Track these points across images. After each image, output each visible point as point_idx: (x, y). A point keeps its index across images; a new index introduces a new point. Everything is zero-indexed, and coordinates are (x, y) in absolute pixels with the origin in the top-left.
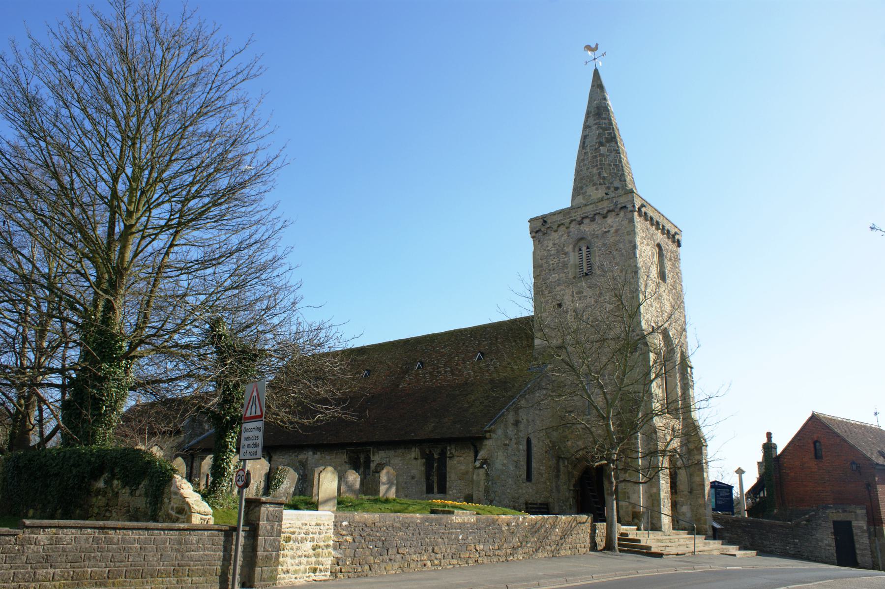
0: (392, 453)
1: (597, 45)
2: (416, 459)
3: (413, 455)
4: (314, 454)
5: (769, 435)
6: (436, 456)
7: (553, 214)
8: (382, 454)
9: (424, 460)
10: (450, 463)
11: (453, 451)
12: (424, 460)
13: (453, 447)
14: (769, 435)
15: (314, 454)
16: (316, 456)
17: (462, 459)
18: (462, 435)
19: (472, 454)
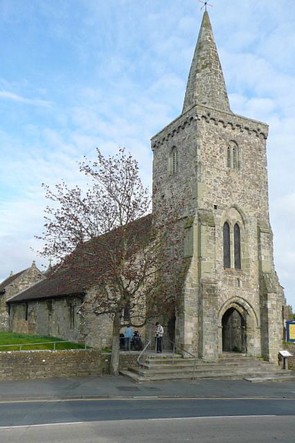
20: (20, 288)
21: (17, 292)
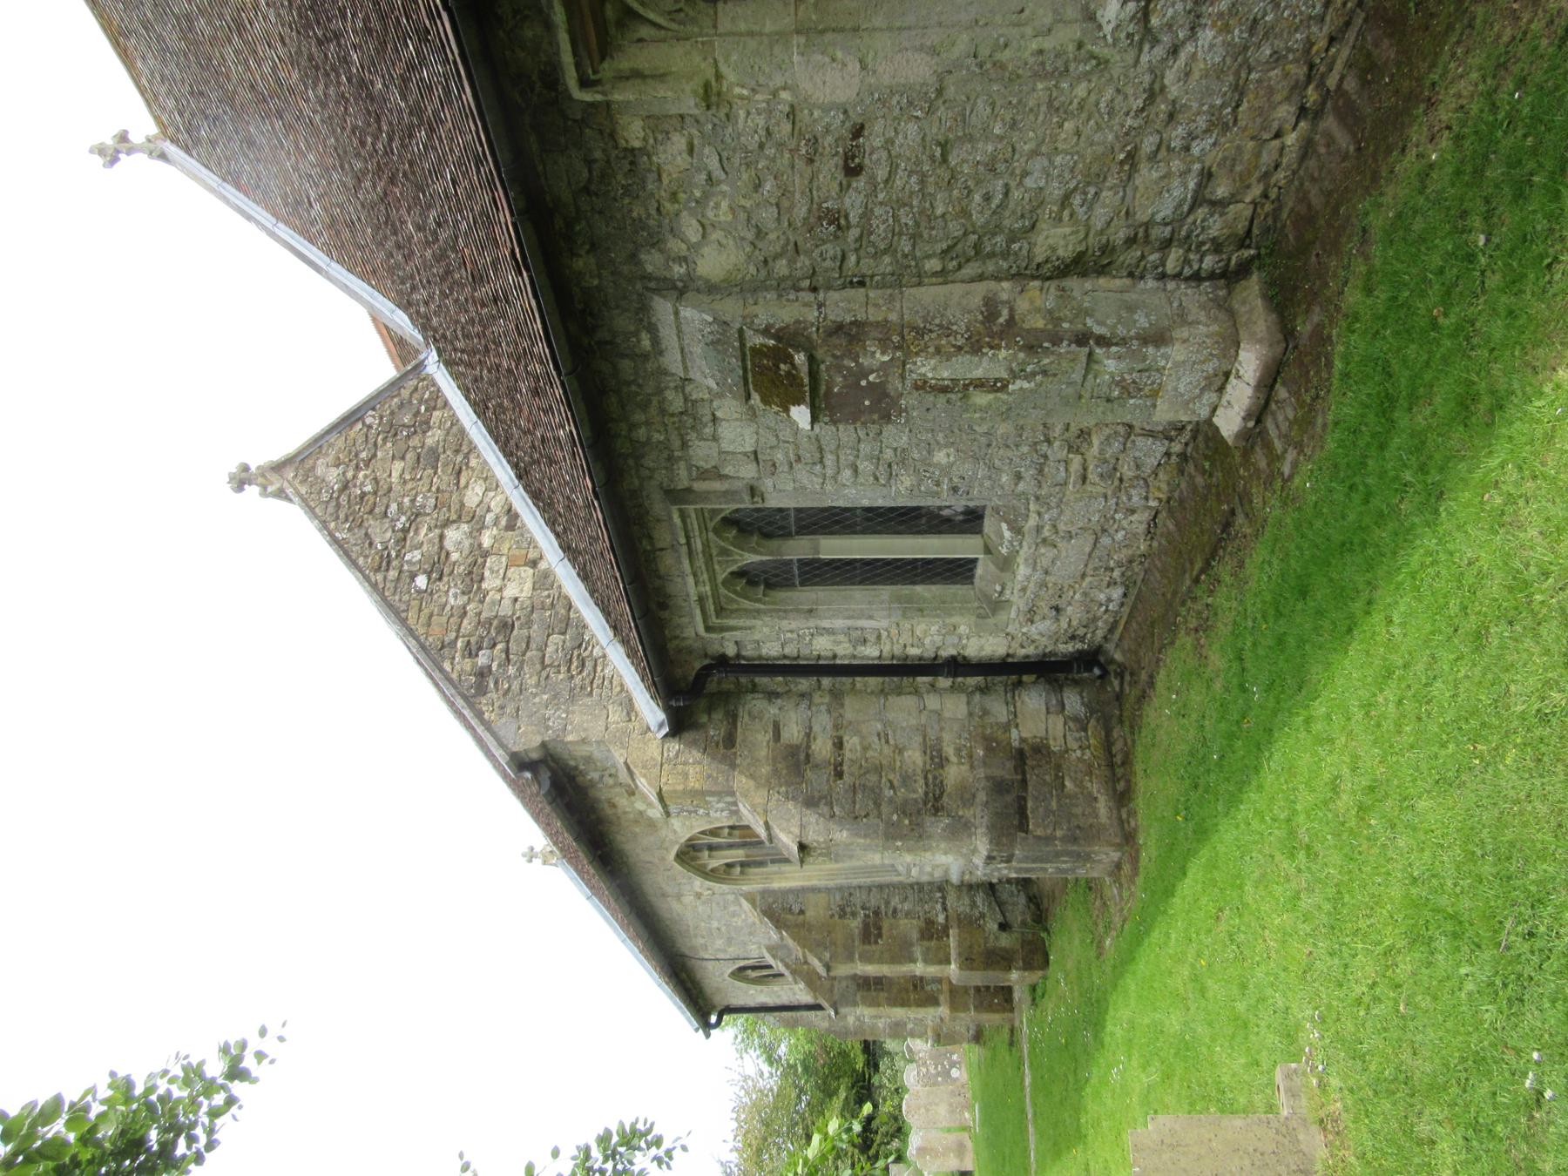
20: (519, 586)
21: (568, 622)
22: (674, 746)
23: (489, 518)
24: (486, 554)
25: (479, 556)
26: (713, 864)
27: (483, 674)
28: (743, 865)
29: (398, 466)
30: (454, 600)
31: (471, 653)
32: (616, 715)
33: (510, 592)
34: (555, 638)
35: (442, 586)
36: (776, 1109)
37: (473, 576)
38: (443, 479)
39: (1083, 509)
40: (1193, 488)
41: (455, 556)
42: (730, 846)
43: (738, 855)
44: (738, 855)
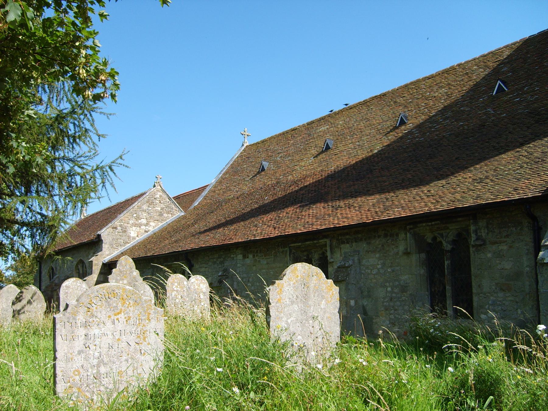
0: (363, 246)
1: (98, 32)
2: (407, 253)
3: (401, 248)
4: (245, 257)
5: (116, 102)
6: (447, 246)
7: (424, 79)
8: (346, 248)
9: (423, 256)
10: (477, 259)
11: (483, 233)
12: (423, 256)
13: (482, 223)
14: (116, 102)
15: (245, 257)
16: (248, 261)
17: (504, 247)
18: (235, 226)
19: (528, 237)
22: (101, 264)
23: (147, 227)
24: (140, 227)
25: (140, 225)
26: (79, 266)
27: (116, 228)
28: (79, 272)
29: (159, 209)
30: (131, 222)
31: (121, 226)
32: (107, 253)
33: (132, 232)
34: (122, 241)
35: (134, 219)
36: (379, 237)
37: (135, 225)
38: (157, 217)
39: (51, 215)
40: (65, 223)
41: (140, 221)
42: (83, 270)
43: (81, 272)
44: (81, 272)
